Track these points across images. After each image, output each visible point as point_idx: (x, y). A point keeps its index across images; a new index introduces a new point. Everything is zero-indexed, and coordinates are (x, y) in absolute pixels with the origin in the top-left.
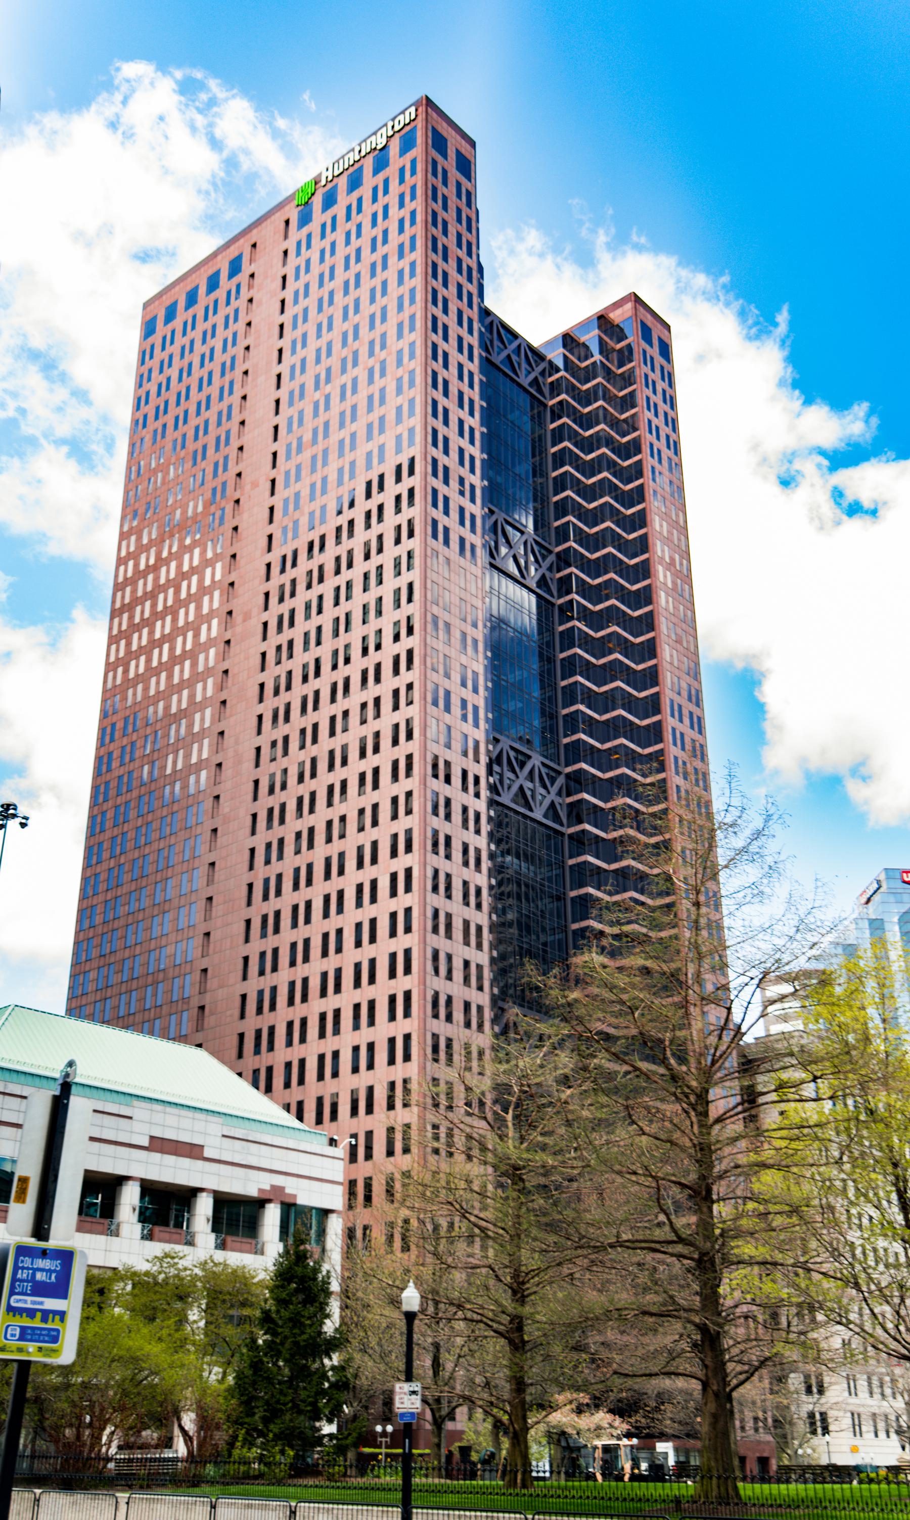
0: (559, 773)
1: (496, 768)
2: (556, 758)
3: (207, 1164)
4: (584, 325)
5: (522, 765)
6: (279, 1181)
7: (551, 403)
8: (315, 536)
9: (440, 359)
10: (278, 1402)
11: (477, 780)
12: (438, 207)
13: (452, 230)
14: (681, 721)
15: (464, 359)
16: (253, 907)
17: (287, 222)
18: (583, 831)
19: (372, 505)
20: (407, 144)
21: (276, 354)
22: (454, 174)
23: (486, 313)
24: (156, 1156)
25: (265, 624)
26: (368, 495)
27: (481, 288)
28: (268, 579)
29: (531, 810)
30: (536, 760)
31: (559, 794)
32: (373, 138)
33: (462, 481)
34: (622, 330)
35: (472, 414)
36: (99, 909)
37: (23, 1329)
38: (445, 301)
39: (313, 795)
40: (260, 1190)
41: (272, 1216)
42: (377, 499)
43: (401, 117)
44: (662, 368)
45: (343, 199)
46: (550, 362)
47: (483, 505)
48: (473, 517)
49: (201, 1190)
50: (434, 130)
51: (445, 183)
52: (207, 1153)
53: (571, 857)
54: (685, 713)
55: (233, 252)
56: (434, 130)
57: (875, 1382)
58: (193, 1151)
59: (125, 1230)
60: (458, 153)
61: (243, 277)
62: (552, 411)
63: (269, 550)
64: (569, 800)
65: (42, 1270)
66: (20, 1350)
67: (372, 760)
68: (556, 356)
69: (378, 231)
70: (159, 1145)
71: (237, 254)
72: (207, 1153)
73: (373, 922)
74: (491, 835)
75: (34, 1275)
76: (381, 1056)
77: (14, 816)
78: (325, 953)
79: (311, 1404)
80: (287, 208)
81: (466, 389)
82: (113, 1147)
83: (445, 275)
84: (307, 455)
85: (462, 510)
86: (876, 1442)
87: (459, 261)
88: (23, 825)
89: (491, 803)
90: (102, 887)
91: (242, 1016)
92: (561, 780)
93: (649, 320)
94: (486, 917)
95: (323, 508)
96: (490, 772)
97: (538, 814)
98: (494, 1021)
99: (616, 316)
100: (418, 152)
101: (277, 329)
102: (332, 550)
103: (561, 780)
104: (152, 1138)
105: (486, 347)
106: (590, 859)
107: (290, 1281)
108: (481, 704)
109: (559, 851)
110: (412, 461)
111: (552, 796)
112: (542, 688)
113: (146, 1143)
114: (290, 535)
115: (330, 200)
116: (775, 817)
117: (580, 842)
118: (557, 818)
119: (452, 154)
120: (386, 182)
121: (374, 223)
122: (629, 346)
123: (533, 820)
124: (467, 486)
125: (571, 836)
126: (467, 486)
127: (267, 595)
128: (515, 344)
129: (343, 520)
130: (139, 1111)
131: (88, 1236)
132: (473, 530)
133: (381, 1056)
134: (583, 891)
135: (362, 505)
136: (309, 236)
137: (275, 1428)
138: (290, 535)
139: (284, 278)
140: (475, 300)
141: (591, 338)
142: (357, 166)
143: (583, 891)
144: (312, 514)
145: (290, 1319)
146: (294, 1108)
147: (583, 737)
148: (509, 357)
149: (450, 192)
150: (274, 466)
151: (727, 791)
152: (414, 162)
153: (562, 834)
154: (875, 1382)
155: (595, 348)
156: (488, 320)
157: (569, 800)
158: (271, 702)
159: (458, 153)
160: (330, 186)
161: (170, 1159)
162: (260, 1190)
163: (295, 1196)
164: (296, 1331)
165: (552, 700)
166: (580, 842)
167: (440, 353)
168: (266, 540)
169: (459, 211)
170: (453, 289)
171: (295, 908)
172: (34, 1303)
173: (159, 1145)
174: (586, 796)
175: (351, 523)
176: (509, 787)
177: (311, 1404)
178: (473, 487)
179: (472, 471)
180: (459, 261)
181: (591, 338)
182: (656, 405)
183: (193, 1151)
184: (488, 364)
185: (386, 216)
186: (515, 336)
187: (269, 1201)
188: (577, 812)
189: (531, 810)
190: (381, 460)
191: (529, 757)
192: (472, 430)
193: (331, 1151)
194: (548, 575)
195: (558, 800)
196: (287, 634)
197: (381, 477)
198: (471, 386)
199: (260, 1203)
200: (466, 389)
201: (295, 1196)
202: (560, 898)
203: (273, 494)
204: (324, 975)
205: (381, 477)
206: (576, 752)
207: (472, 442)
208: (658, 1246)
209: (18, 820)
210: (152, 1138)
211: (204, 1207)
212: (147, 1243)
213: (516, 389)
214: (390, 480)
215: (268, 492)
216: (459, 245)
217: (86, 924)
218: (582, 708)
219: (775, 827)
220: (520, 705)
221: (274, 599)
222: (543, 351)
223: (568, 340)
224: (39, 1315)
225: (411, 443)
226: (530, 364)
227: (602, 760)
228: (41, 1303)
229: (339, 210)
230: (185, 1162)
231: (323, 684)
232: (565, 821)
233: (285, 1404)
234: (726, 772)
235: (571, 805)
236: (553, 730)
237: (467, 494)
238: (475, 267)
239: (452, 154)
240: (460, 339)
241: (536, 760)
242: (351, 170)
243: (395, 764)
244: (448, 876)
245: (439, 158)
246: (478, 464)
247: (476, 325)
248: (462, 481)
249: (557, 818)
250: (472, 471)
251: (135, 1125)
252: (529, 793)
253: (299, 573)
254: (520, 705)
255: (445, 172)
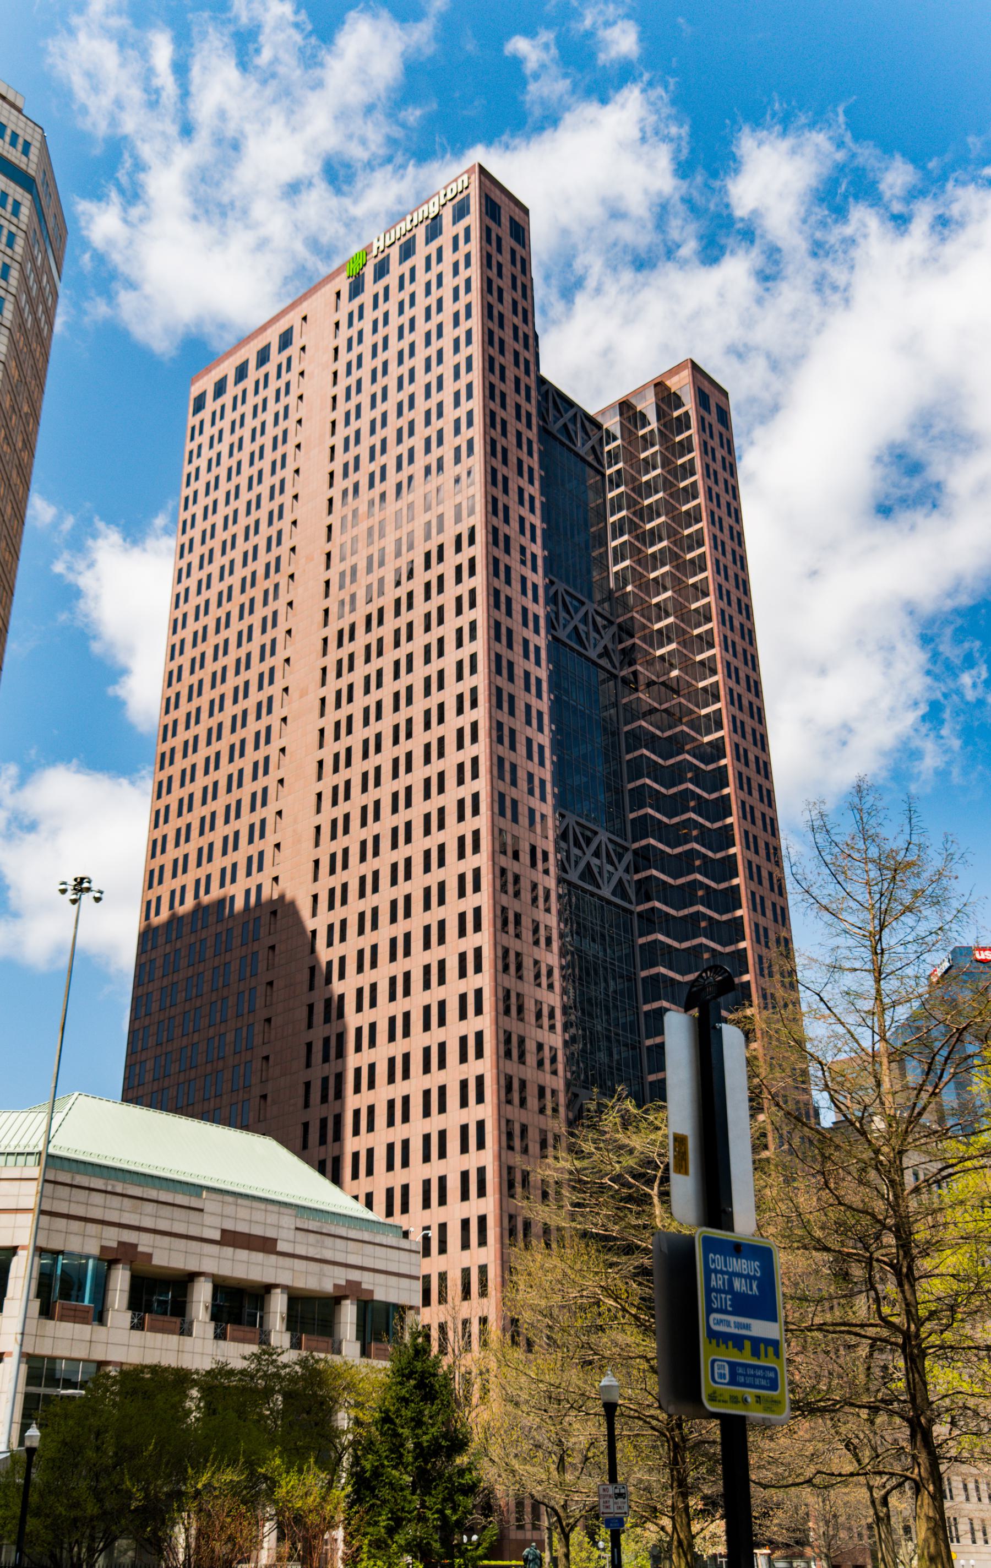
0: (627, 849)
1: (563, 845)
2: (622, 833)
3: (281, 1259)
4: (639, 392)
5: (588, 841)
6: (355, 1275)
7: (608, 472)
8: (373, 609)
9: (499, 427)
10: (403, 1509)
11: (545, 855)
12: (493, 274)
13: (507, 297)
14: (750, 793)
15: (522, 427)
16: (316, 992)
17: (338, 294)
18: (653, 909)
19: (432, 575)
20: (461, 211)
21: (329, 426)
22: (508, 242)
23: (542, 381)
24: (229, 1251)
25: (323, 700)
26: (428, 566)
27: (537, 355)
28: (325, 654)
29: (599, 887)
30: (603, 836)
31: (627, 870)
32: (425, 207)
33: (523, 550)
34: (679, 398)
35: (531, 482)
36: (156, 996)
37: (733, 1366)
38: (503, 369)
39: (376, 874)
40: (336, 1286)
41: (348, 1313)
42: (436, 569)
43: (454, 186)
44: (721, 435)
45: (396, 269)
46: (607, 431)
47: (545, 575)
48: (535, 587)
49: (276, 1286)
50: (487, 197)
51: (499, 250)
52: (281, 1247)
53: (641, 936)
54: (755, 786)
55: (282, 326)
56: (487, 197)
57: (971, 1486)
58: (266, 1245)
59: (196, 1329)
60: (512, 220)
61: (293, 350)
62: (611, 481)
63: (326, 624)
64: (637, 877)
65: (739, 1275)
66: (734, 1400)
67: (437, 837)
68: (612, 423)
69: (379, 338)
70: (231, 1239)
71: (286, 327)
72: (281, 1247)
73: (442, 1004)
74: (560, 913)
75: (731, 1283)
76: (453, 1144)
77: (88, 889)
78: (427, 1027)
79: (437, 1511)
80: (338, 280)
81: (525, 457)
82: (184, 1241)
83: (502, 342)
84: (363, 526)
85: (524, 580)
86: (973, 1548)
87: (516, 329)
88: (98, 900)
89: (560, 881)
90: (158, 973)
91: (307, 1105)
92: (628, 857)
93: (707, 388)
94: (558, 998)
95: (381, 581)
96: (558, 850)
97: (606, 892)
98: (569, 1106)
99: (674, 384)
100: (473, 219)
101: (330, 401)
102: (391, 622)
103: (628, 857)
104: (224, 1232)
105: (542, 416)
106: (661, 937)
107: (409, 1377)
108: (548, 777)
109: (628, 929)
110: (472, 530)
111: (620, 873)
112: (607, 761)
113: (217, 1236)
114: (347, 608)
115: (382, 270)
116: (956, 857)
117: (650, 921)
118: (625, 896)
119: (505, 221)
120: (440, 251)
121: (428, 292)
122: (687, 413)
123: (601, 898)
124: (529, 556)
125: (640, 915)
126: (529, 556)
127: (324, 670)
128: (571, 413)
129: (402, 592)
130: (210, 1204)
131: (159, 1336)
132: (535, 600)
133: (453, 1144)
134: (654, 971)
135: (421, 576)
136: (361, 308)
137: (400, 1539)
138: (347, 608)
139: (336, 350)
140: (532, 367)
141: (648, 406)
142: (409, 236)
143: (654, 971)
144: (369, 587)
145: (412, 1419)
146: (362, 1198)
147: (650, 811)
148: (565, 426)
149: (505, 258)
150: (329, 539)
151: (907, 829)
152: (467, 230)
153: (632, 913)
154: (971, 1486)
155: (652, 416)
156: (544, 388)
157: (637, 877)
158: (330, 780)
159: (512, 220)
160: (381, 256)
161: (243, 1254)
162: (336, 1286)
163: (372, 1292)
164: (419, 1431)
165: (617, 774)
166: (650, 921)
167: (498, 420)
168: (322, 614)
169: (514, 278)
170: (510, 357)
171: (360, 992)
172: (738, 1326)
173: (231, 1239)
174: (655, 872)
175: (410, 595)
176: (576, 863)
177: (437, 1511)
178: (534, 557)
179: (533, 540)
180: (516, 329)
181: (648, 406)
182: (715, 473)
183: (266, 1245)
184: (545, 432)
185: (440, 284)
186: (570, 404)
187: (346, 1297)
188: (646, 890)
189: (599, 887)
190: (440, 530)
191: (596, 833)
192: (532, 498)
193: (404, 1244)
194: (610, 646)
195: (626, 877)
196: (346, 709)
197: (441, 548)
198: (530, 453)
199: (336, 1300)
200: (525, 457)
201: (372, 1292)
202: (632, 978)
203: (328, 567)
204: (392, 1061)
205: (441, 548)
206: (644, 827)
207: (532, 510)
208: (857, 1329)
209: (91, 894)
210: (224, 1232)
211: (278, 1304)
212: (221, 1343)
213: (573, 457)
214: (449, 550)
215: (323, 566)
216: (515, 312)
217: (142, 1011)
218: (648, 781)
219: (957, 868)
220: (584, 779)
221: (331, 674)
222: (599, 419)
223: (625, 407)
224: (747, 1344)
225: (471, 512)
226: (587, 433)
227: (673, 835)
228: (748, 1327)
229: (391, 279)
230: (259, 1257)
231: (384, 760)
232: (633, 898)
233: (410, 1512)
234: (905, 807)
235: (639, 882)
236: (619, 805)
237: (529, 563)
238: (531, 335)
239: (505, 221)
240: (518, 407)
241: (603, 836)
242: (403, 240)
243: (461, 840)
244: (518, 955)
245: (493, 226)
246: (539, 533)
247: (533, 393)
248: (523, 550)
249: (625, 896)
250: (533, 540)
251: (208, 1219)
252: (596, 870)
253: (358, 647)
254: (584, 779)
255: (499, 239)
